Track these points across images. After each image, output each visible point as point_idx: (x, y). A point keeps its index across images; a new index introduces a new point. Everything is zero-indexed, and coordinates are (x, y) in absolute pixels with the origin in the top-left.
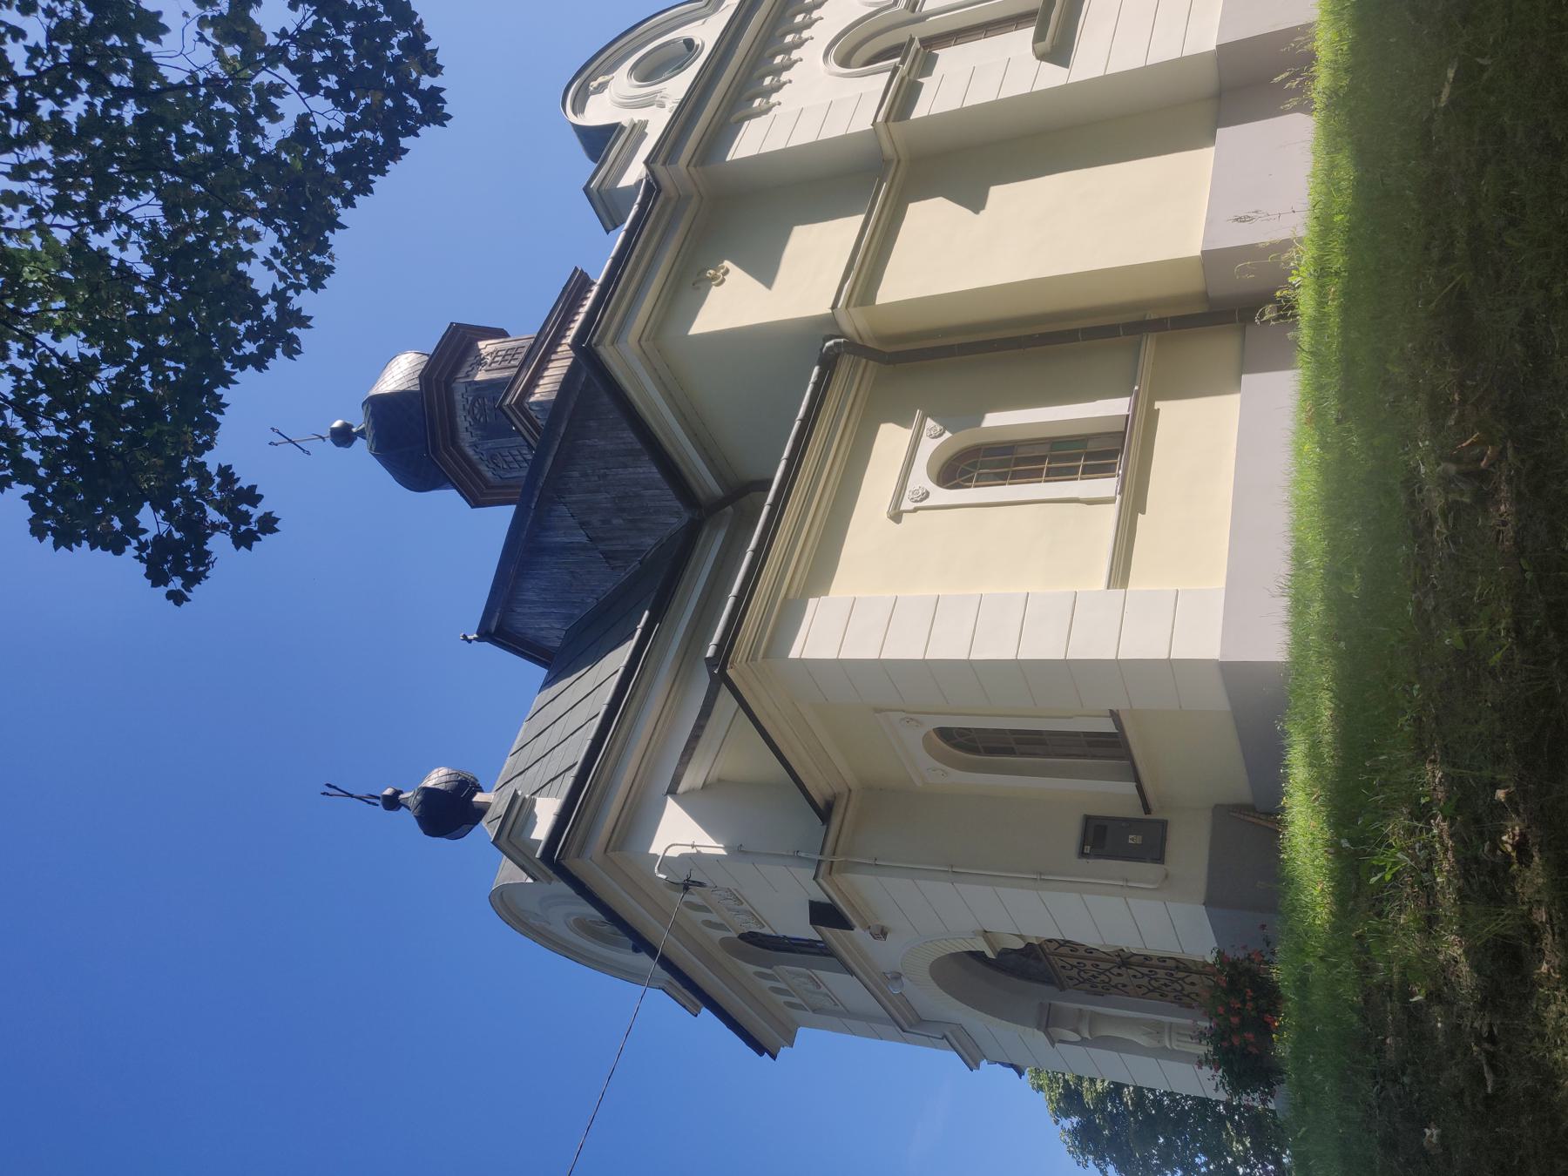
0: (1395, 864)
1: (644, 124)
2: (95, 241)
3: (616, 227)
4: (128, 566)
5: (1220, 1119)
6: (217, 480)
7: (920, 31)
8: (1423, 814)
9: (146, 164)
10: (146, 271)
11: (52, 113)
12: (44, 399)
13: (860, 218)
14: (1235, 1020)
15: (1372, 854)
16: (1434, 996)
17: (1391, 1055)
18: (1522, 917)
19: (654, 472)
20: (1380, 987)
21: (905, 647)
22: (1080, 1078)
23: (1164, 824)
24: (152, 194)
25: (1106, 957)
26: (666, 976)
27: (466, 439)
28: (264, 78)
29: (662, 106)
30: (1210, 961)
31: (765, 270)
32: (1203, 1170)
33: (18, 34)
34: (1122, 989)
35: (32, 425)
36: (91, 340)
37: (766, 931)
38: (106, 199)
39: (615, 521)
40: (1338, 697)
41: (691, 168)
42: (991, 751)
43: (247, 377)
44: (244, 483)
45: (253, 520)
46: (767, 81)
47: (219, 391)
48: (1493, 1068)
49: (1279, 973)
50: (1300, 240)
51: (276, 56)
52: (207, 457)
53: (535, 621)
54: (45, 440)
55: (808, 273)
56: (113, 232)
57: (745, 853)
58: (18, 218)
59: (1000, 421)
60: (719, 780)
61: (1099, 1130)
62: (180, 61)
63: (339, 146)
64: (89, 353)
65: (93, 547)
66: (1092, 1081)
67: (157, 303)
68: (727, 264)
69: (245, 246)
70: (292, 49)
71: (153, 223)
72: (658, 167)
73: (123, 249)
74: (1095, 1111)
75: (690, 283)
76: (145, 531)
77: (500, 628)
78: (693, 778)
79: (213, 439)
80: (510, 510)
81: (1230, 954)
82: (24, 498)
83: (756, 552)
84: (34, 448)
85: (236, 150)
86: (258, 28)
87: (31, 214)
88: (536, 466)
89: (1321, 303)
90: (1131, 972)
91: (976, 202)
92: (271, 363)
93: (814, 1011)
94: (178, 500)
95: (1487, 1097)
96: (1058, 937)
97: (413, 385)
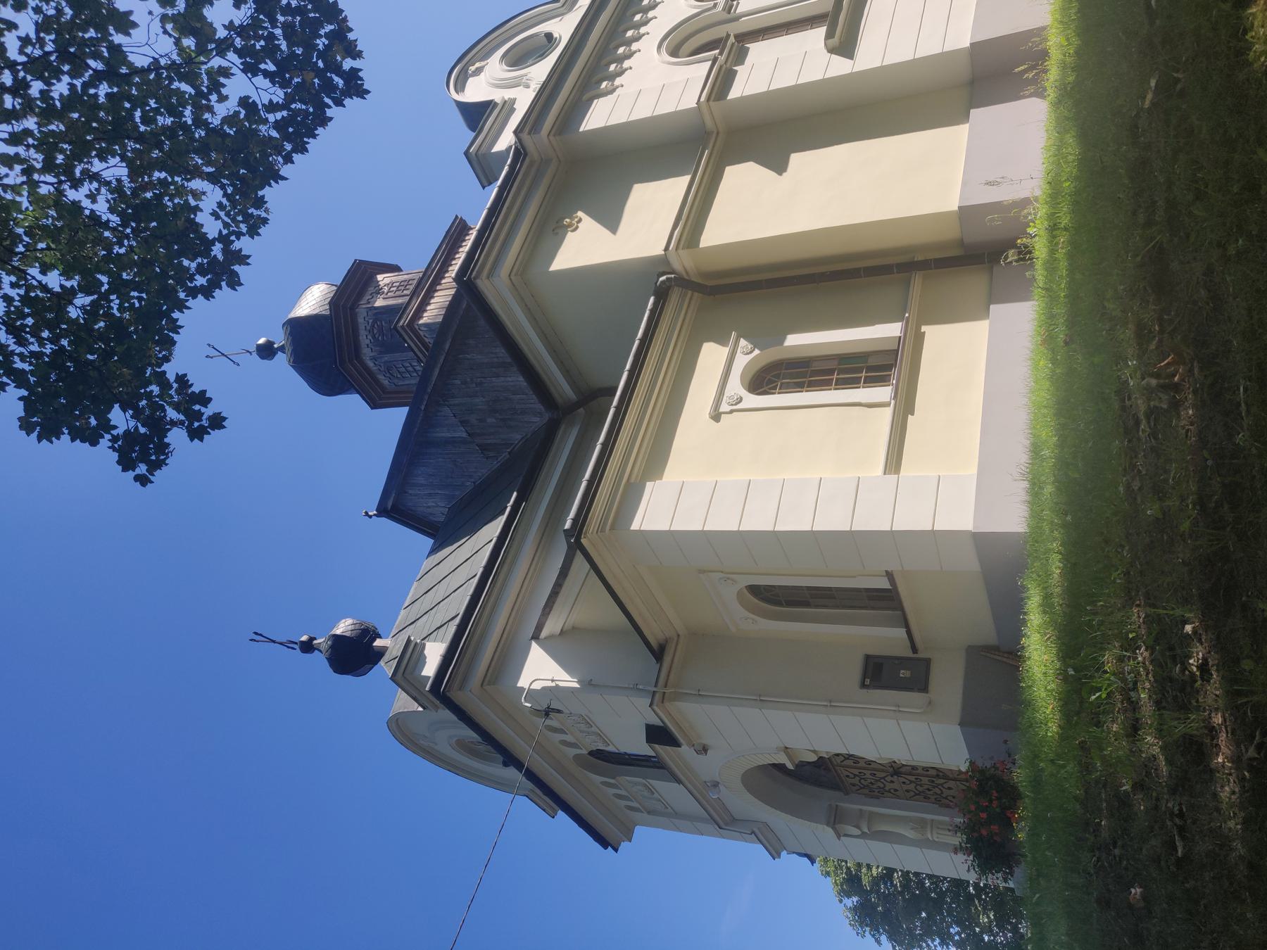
0: (1109, 685)
1: (513, 101)
2: (72, 195)
3: (490, 183)
4: (104, 453)
5: (970, 898)
6: (175, 385)
7: (734, 29)
8: (1131, 646)
9: (115, 133)
10: (115, 219)
11: (41, 92)
12: (30, 321)
13: (687, 178)
14: (984, 815)
15: (1092, 677)
16: (1138, 786)
17: (1105, 834)
18: (1204, 721)
19: (521, 380)
20: (1097, 782)
21: (724, 520)
22: (859, 865)
23: (928, 662)
24: (118, 159)
25: (882, 768)
26: (530, 785)
27: (367, 353)
28: (216, 62)
29: (528, 87)
30: (963, 769)
31: (611, 221)
32: (957, 938)
33: (12, 26)
34: (894, 793)
35: (21, 342)
36: (67, 274)
37: (611, 748)
38: (81, 161)
39: (489, 420)
40: (1066, 558)
41: (551, 138)
42: (790, 604)
43: (198, 304)
44: (196, 389)
45: (204, 417)
46: (612, 67)
47: (176, 315)
48: (1183, 838)
49: (1020, 776)
50: (1036, 199)
51: (223, 47)
52: (165, 367)
53: (426, 498)
54: (32, 354)
55: (645, 222)
56: (85, 189)
57: (595, 686)
58: (14, 176)
59: (798, 341)
60: (573, 628)
61: (874, 907)
62: (146, 50)
63: (279, 115)
64: (68, 284)
65: (73, 440)
66: (869, 867)
67: (121, 245)
68: (580, 214)
69: (193, 203)
70: (238, 40)
71: (119, 181)
72: (525, 136)
73: (94, 201)
74: (871, 892)
75: (551, 229)
76: (115, 427)
77: (395, 506)
78: (553, 626)
79: (171, 354)
80: (407, 409)
81: (980, 764)
82: (20, 399)
83: (604, 445)
84: (23, 360)
85: (190, 122)
86: (211, 24)
87: (24, 172)
88: (425, 378)
89: (1052, 252)
90: (902, 780)
91: (779, 166)
92: (217, 293)
93: (649, 813)
94: (144, 402)
95: (1179, 861)
96: (844, 751)
97: (324, 310)
